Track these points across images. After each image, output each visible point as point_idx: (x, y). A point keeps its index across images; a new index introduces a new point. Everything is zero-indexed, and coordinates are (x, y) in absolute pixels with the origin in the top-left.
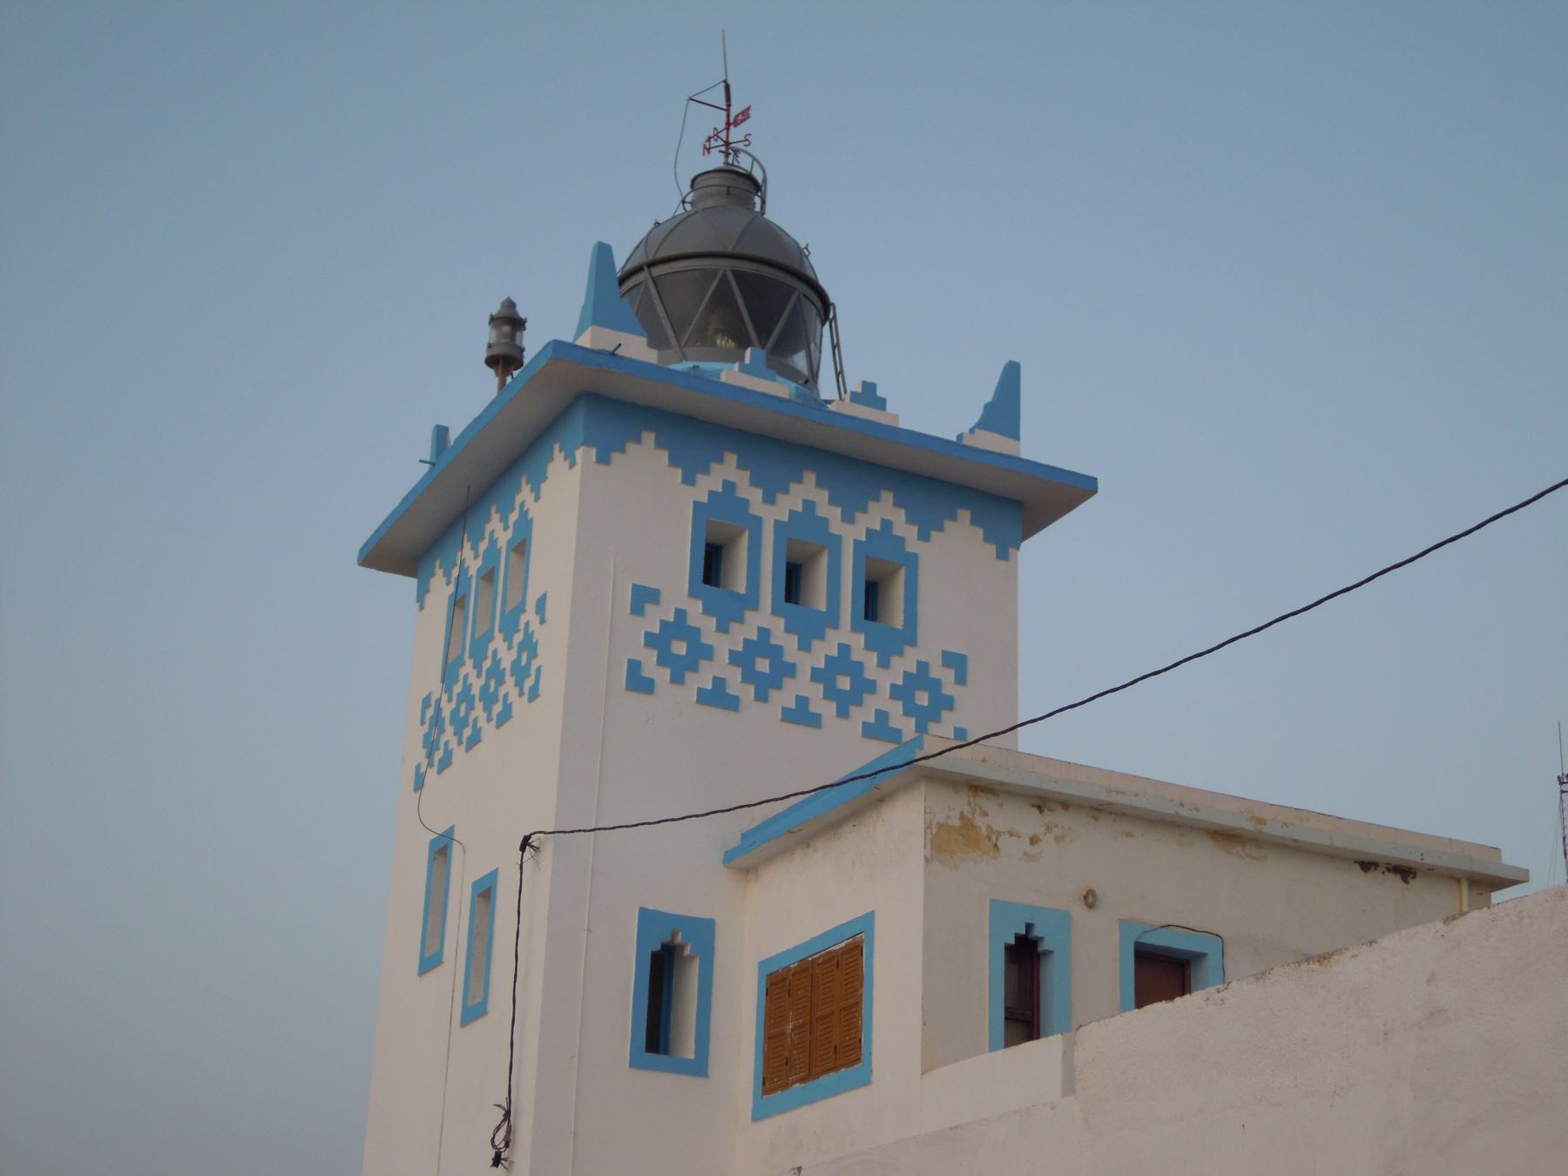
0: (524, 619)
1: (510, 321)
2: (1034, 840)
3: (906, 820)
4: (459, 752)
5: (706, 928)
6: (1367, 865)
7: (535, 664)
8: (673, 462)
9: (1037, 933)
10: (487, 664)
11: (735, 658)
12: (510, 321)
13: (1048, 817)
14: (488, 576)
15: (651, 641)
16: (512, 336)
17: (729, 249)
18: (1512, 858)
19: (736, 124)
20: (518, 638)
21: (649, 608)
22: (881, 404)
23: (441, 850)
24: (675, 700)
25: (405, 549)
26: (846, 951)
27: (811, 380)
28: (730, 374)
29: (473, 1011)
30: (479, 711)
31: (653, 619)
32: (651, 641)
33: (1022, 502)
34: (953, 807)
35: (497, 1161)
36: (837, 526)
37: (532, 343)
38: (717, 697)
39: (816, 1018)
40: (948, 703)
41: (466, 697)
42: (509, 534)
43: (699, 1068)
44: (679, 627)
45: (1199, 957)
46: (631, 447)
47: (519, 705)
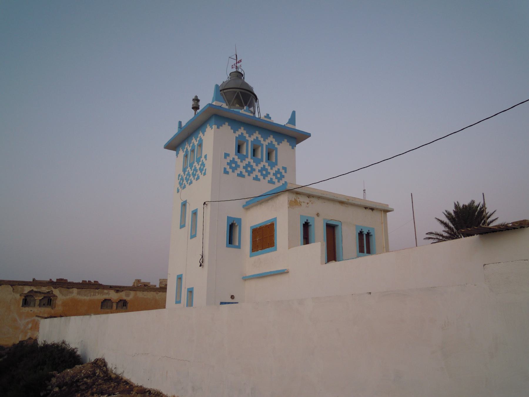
0: (201, 159)
1: (196, 100)
2: (308, 203)
3: (284, 200)
4: (187, 186)
5: (239, 220)
6: (366, 208)
7: (204, 168)
8: (231, 129)
9: (309, 221)
10: (193, 168)
11: (244, 168)
12: (196, 100)
13: (310, 199)
14: (193, 151)
15: (228, 164)
16: (197, 103)
17: (239, 87)
18: (390, 207)
19: (238, 62)
20: (200, 163)
21: (228, 157)
22: (270, 118)
23: (184, 204)
24: (233, 175)
25: (174, 145)
26: (270, 225)
27: (254, 113)
28: (242, 111)
29: (193, 236)
30: (192, 177)
31: (228, 160)
32: (228, 164)
33: (296, 137)
34: (293, 197)
35: (201, 265)
36: (262, 142)
37: (202, 105)
38: (241, 175)
39: (264, 238)
40: (283, 177)
41: (188, 174)
42: (197, 142)
43: (239, 247)
44: (233, 161)
45: (337, 226)
46: (223, 125)
47: (201, 176)
